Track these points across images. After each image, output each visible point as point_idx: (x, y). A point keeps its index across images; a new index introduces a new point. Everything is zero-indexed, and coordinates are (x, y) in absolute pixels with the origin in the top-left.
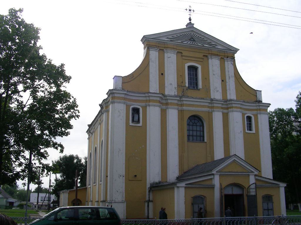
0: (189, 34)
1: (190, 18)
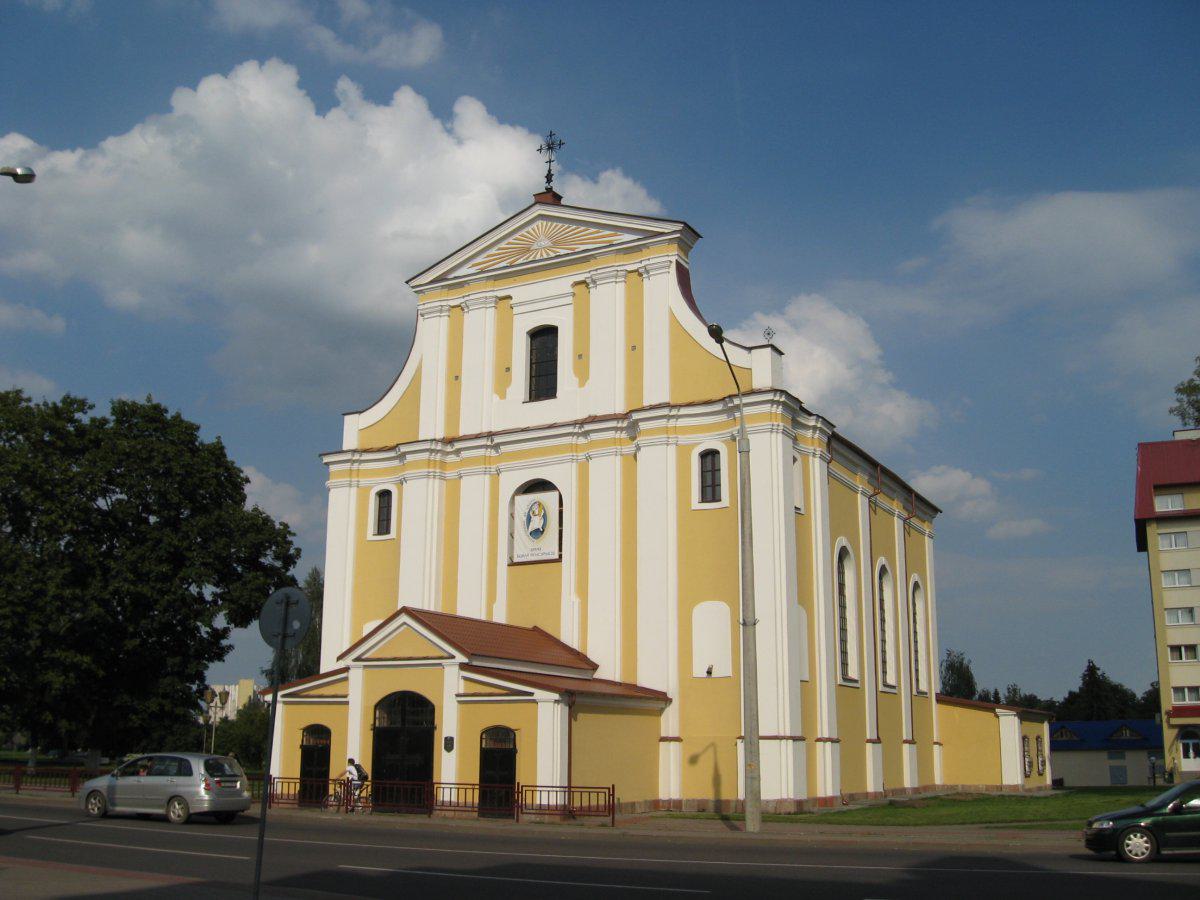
0: (528, 232)
1: (549, 171)
